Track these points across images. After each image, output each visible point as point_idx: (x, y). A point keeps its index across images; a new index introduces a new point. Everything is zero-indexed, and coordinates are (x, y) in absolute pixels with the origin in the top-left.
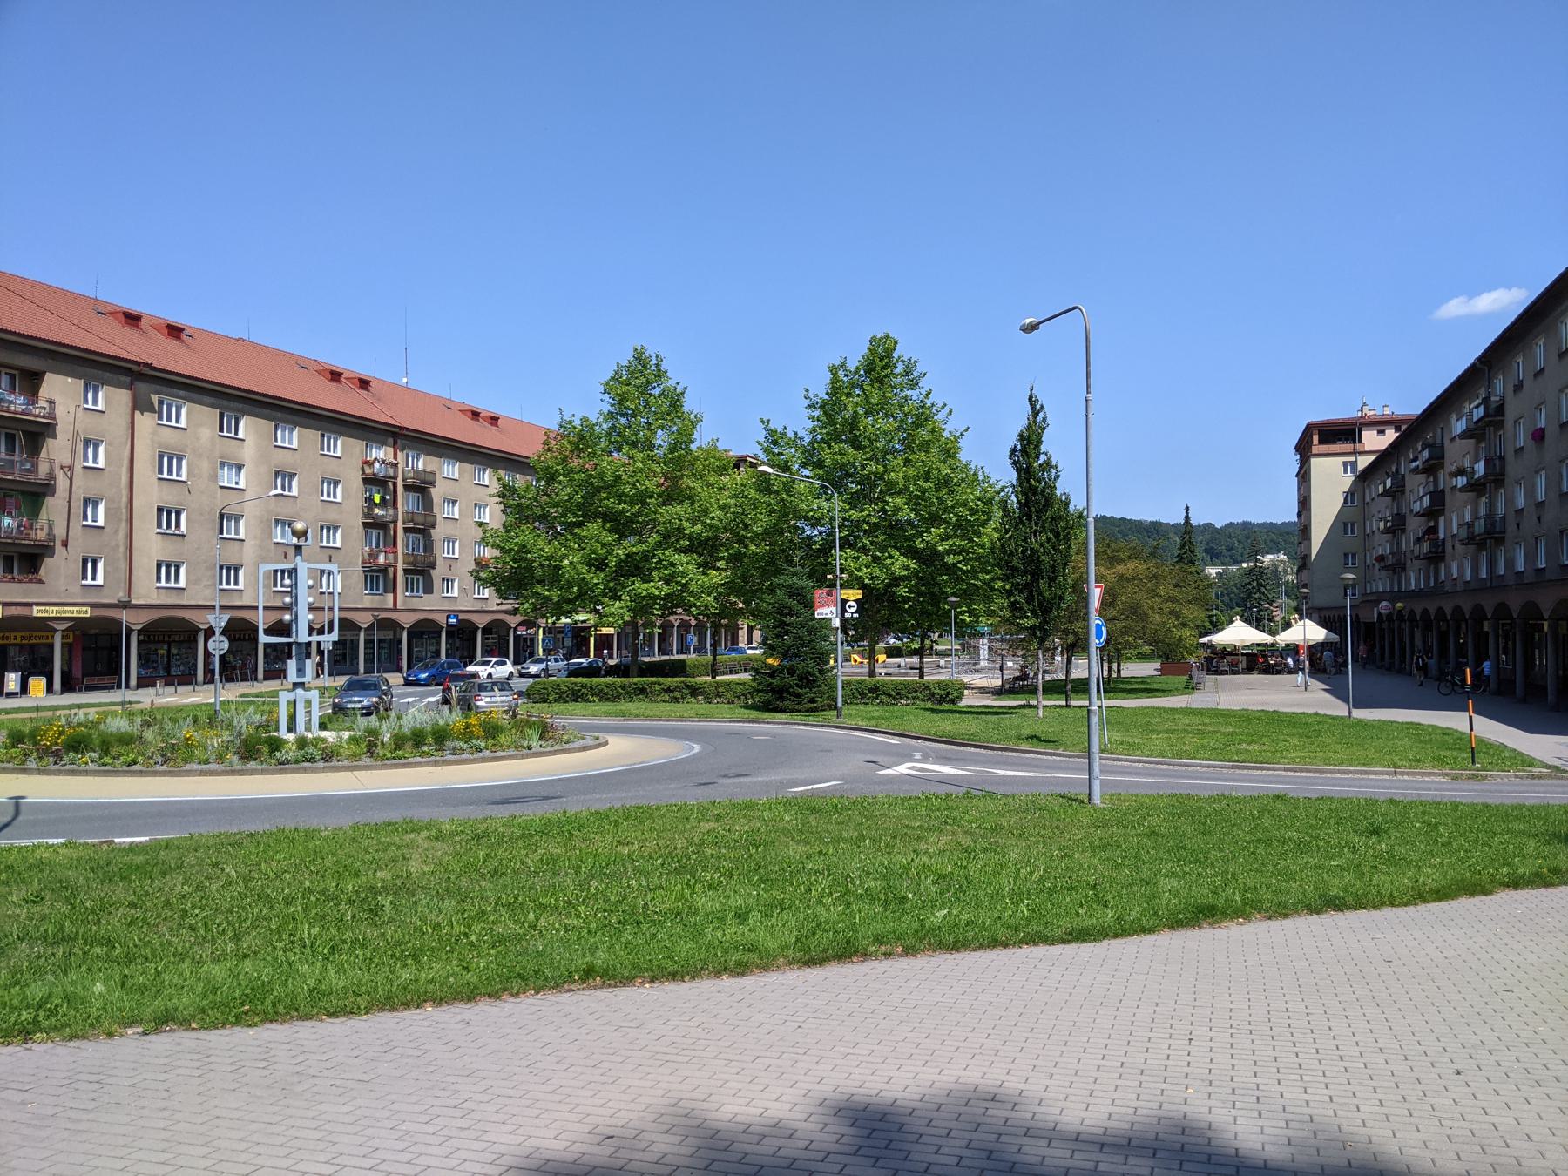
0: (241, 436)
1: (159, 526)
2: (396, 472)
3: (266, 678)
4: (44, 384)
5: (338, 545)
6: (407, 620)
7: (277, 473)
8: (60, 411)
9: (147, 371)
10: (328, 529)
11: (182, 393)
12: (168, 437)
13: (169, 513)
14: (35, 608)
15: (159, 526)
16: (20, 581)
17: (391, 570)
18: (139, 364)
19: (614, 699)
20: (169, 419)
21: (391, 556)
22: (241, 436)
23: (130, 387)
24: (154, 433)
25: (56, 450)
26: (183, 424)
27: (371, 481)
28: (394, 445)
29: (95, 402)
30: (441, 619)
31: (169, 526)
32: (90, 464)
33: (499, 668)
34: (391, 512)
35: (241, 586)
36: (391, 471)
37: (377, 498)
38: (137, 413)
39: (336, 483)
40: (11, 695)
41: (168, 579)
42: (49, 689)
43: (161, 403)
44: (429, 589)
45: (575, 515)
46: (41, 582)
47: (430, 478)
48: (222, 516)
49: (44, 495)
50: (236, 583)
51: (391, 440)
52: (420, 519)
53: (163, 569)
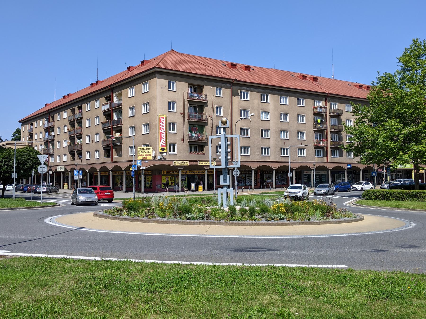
0: (268, 102)
1: (241, 134)
2: (326, 110)
3: (276, 188)
4: (204, 90)
5: (305, 139)
6: (330, 167)
7: (281, 114)
8: (209, 98)
9: (235, 82)
10: (301, 133)
11: (248, 88)
12: (244, 104)
13: (244, 130)
14: (199, 162)
15: (241, 134)
16: (198, 154)
17: (325, 148)
18: (232, 80)
19: (403, 199)
20: (244, 98)
21: (325, 142)
22: (268, 102)
23: (230, 88)
24: (239, 103)
25: (208, 111)
26: (248, 99)
27: (317, 115)
28: (326, 101)
29: (220, 94)
30: (344, 166)
31: (244, 134)
32: (218, 115)
33: (366, 186)
34: (325, 126)
35: (269, 155)
36: (325, 110)
37: (319, 121)
38: (233, 97)
39: (303, 116)
40: (193, 191)
41: (245, 153)
42: (204, 189)
43: (241, 92)
44: (341, 155)
45: (383, 116)
46: (204, 154)
47: (340, 112)
48: (262, 130)
49: (204, 126)
50: (268, 154)
51: (324, 99)
52: (336, 128)
53: (243, 149)
